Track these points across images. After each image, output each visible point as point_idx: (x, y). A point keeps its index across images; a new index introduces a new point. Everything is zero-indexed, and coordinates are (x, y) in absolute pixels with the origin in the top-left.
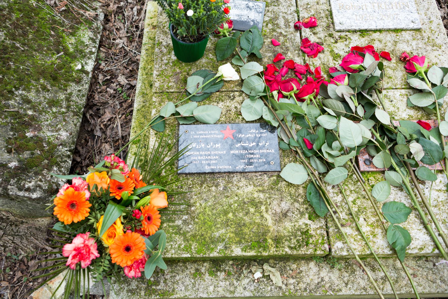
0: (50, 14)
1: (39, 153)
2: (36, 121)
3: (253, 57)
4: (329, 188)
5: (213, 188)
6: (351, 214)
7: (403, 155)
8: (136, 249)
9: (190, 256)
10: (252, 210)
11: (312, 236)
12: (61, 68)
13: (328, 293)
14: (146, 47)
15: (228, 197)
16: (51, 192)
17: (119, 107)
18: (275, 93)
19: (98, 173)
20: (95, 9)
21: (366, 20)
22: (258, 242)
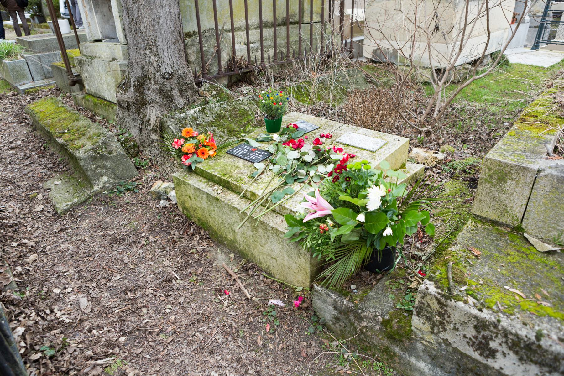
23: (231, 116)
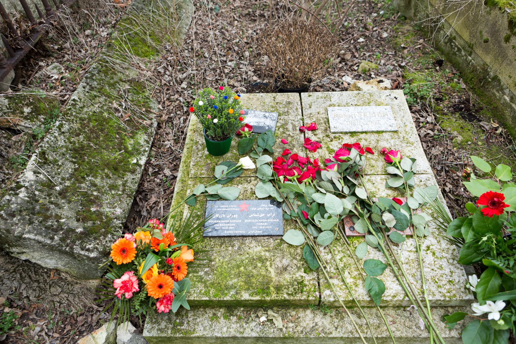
0: (117, 123)
1: (99, 223)
2: (99, 199)
3: (266, 151)
4: (321, 249)
5: (230, 248)
6: (338, 269)
7: (379, 223)
8: (167, 287)
9: (208, 299)
10: (259, 265)
11: (306, 286)
12: (121, 162)
13: (321, 335)
14: (188, 146)
15: (241, 255)
16: (104, 254)
17: (163, 193)
18: (282, 178)
19: (143, 232)
20: (151, 119)
21: (355, 125)
22: (263, 290)
23: (89, 139)
